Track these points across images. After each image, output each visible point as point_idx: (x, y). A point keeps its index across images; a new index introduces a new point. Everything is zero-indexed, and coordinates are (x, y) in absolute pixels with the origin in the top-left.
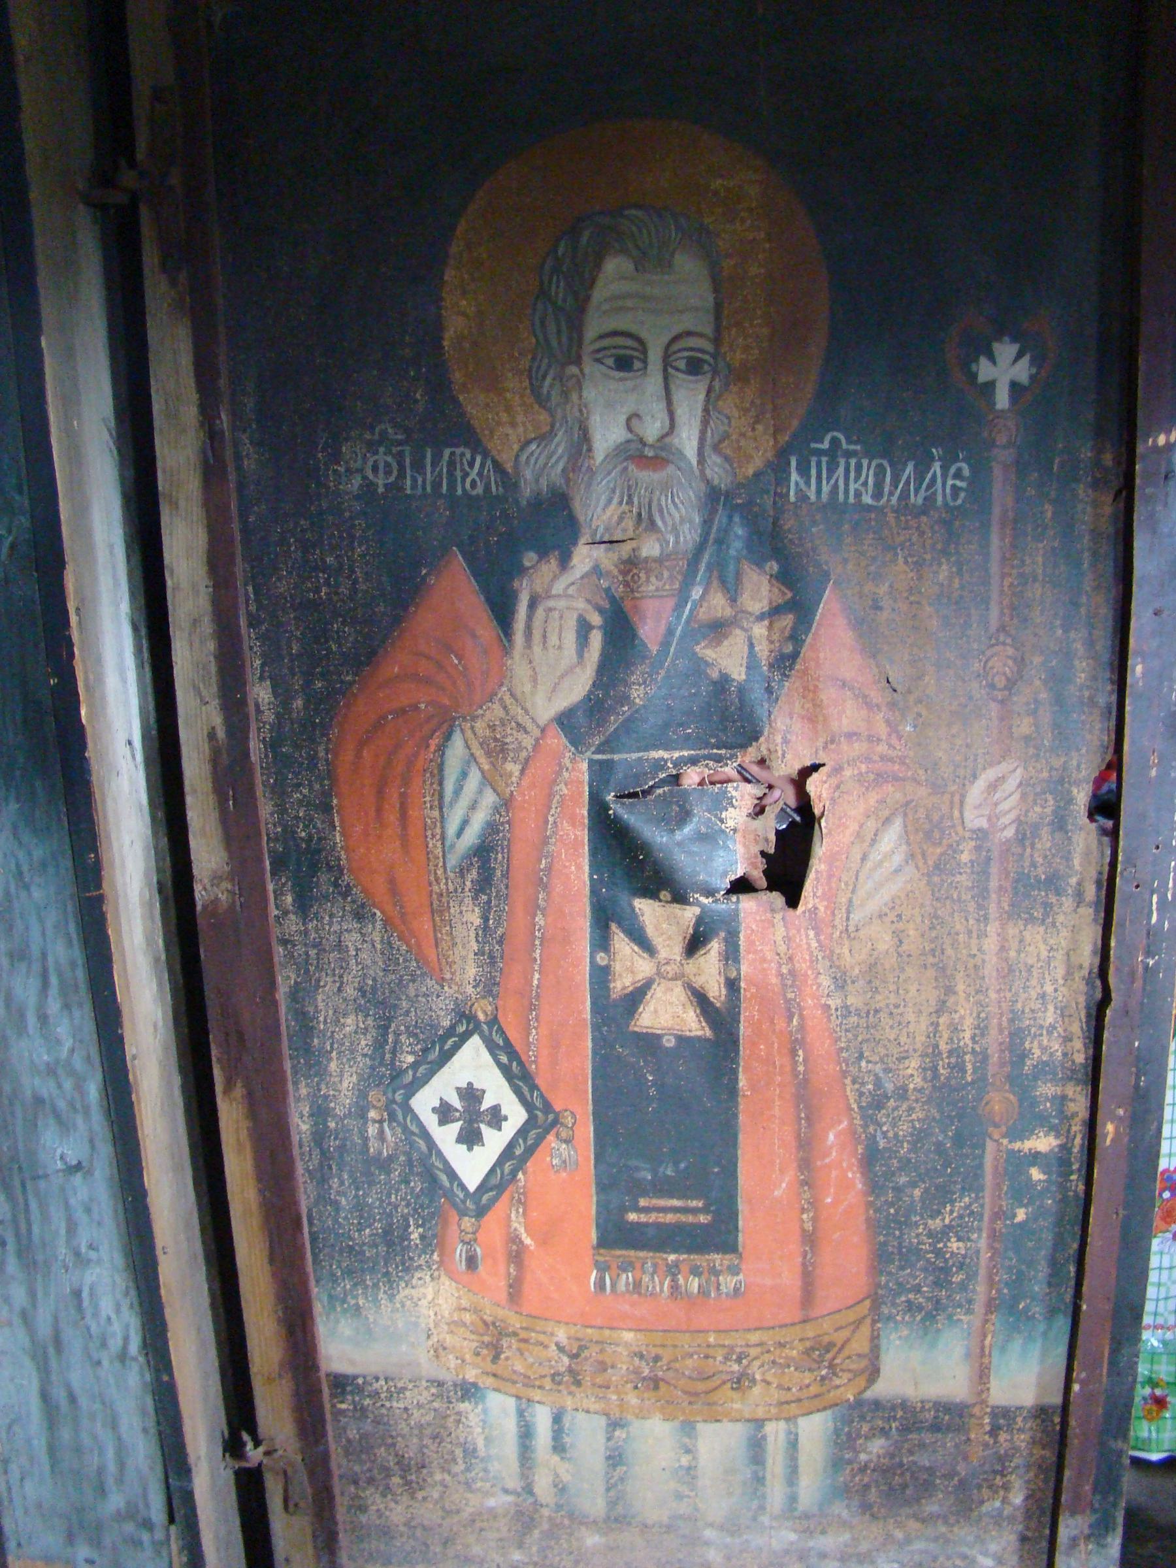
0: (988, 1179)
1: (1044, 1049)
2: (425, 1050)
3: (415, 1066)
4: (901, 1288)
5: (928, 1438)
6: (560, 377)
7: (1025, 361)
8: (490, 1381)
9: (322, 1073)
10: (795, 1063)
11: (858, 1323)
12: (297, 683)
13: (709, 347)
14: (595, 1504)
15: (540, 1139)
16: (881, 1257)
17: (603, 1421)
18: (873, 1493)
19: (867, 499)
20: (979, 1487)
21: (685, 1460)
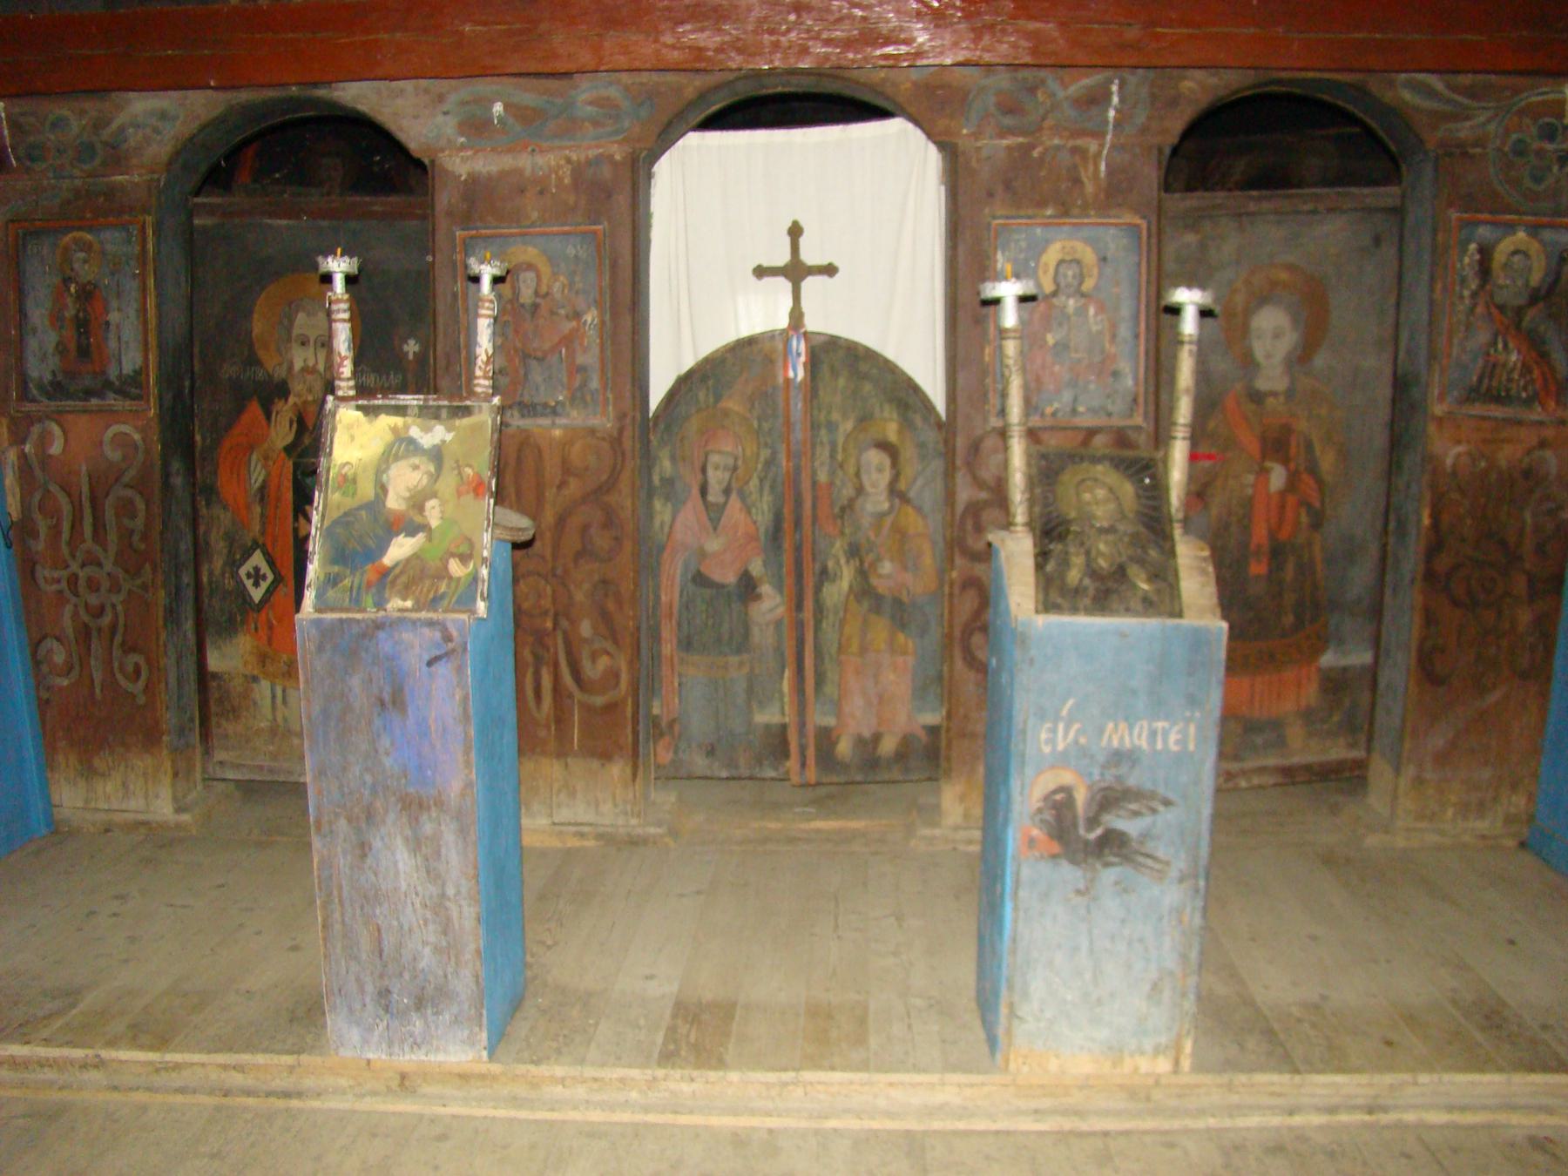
9: (211, 562)
12: (208, 435)
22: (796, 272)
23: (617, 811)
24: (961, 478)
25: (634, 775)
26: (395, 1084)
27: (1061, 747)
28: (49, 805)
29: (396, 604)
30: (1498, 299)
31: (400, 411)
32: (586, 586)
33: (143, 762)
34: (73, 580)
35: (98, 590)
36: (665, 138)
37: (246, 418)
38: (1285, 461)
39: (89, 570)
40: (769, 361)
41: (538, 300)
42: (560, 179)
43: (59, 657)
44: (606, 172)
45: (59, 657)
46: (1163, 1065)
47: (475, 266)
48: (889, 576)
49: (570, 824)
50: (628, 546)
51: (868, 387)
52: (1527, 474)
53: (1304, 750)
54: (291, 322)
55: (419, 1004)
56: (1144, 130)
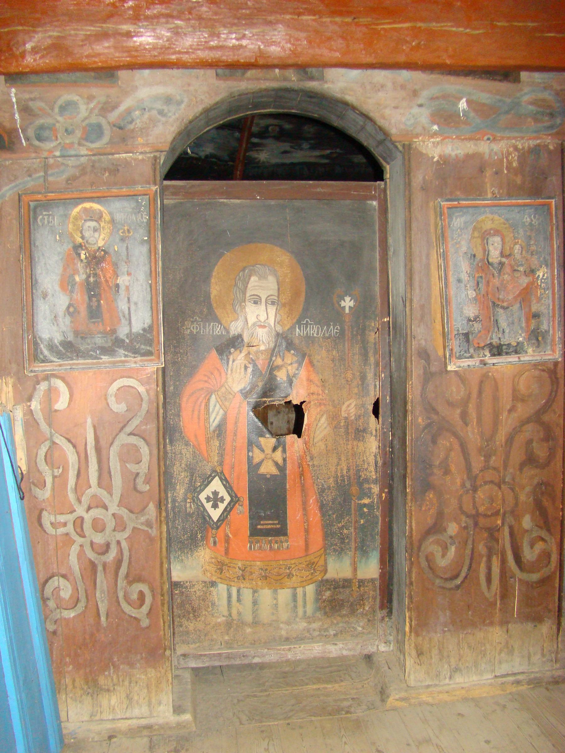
0: (353, 512)
1: (365, 475)
2: (203, 482)
3: (200, 486)
4: (332, 545)
5: (341, 590)
6: (240, 305)
7: (353, 301)
8: (219, 580)
9: (175, 489)
10: (301, 480)
11: (321, 556)
13: (277, 298)
14: (248, 618)
15: (234, 505)
16: (326, 536)
17: (251, 591)
18: (327, 609)
19: (315, 335)
20: (356, 605)
21: (275, 602)
23: (544, 659)
32: (528, 489)
34: (79, 523)
35: (103, 530)
39: (96, 513)
41: (504, 260)
42: (510, 163)
43: (66, 593)
49: (508, 675)
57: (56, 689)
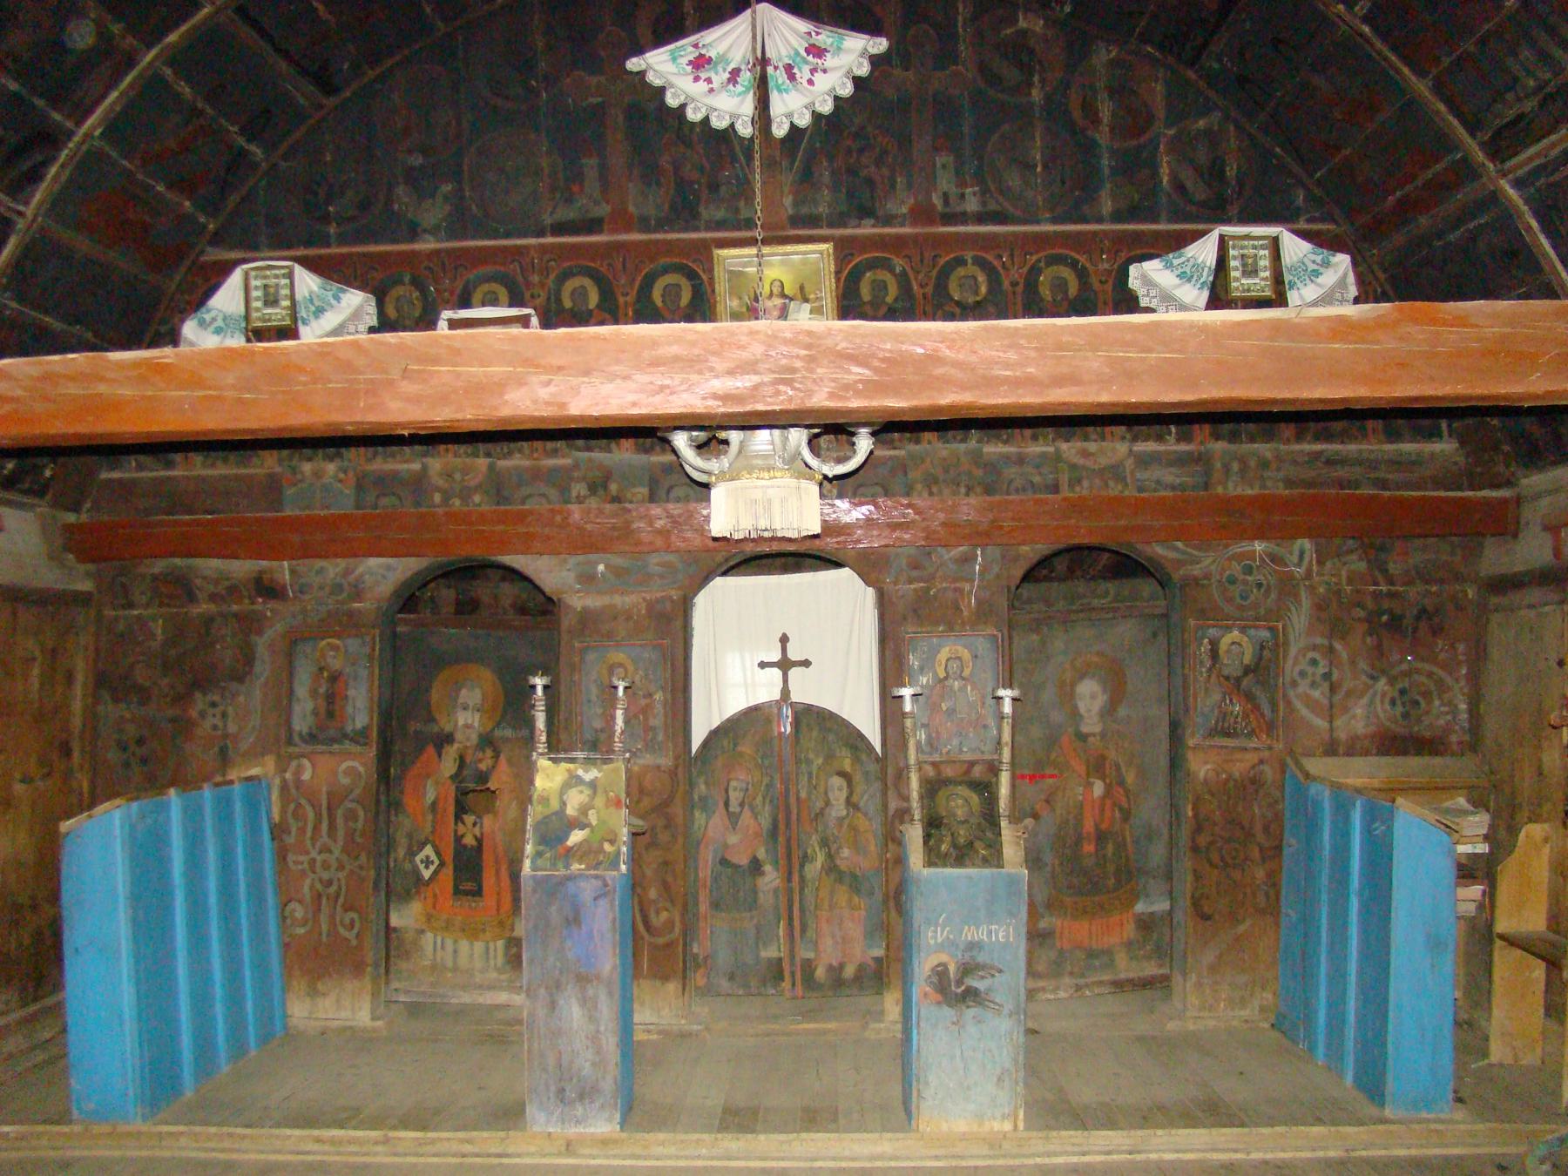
14: (450, 964)
22: (785, 665)
24: (891, 793)
25: (684, 989)
26: (563, 1149)
27: (939, 940)
28: (285, 1016)
29: (576, 866)
30: (1226, 672)
31: (572, 760)
32: (654, 866)
33: (351, 985)
36: (706, 579)
37: (424, 757)
38: (1103, 778)
39: (324, 856)
40: (768, 721)
42: (639, 610)
43: (299, 914)
44: (668, 606)
45: (299, 914)
46: (1007, 1126)
47: (616, 682)
48: (846, 858)
50: (680, 840)
51: (831, 737)
52: (1253, 781)
53: (1126, 968)
54: (458, 696)
55: (581, 1097)
56: (998, 576)
57: (286, 989)
